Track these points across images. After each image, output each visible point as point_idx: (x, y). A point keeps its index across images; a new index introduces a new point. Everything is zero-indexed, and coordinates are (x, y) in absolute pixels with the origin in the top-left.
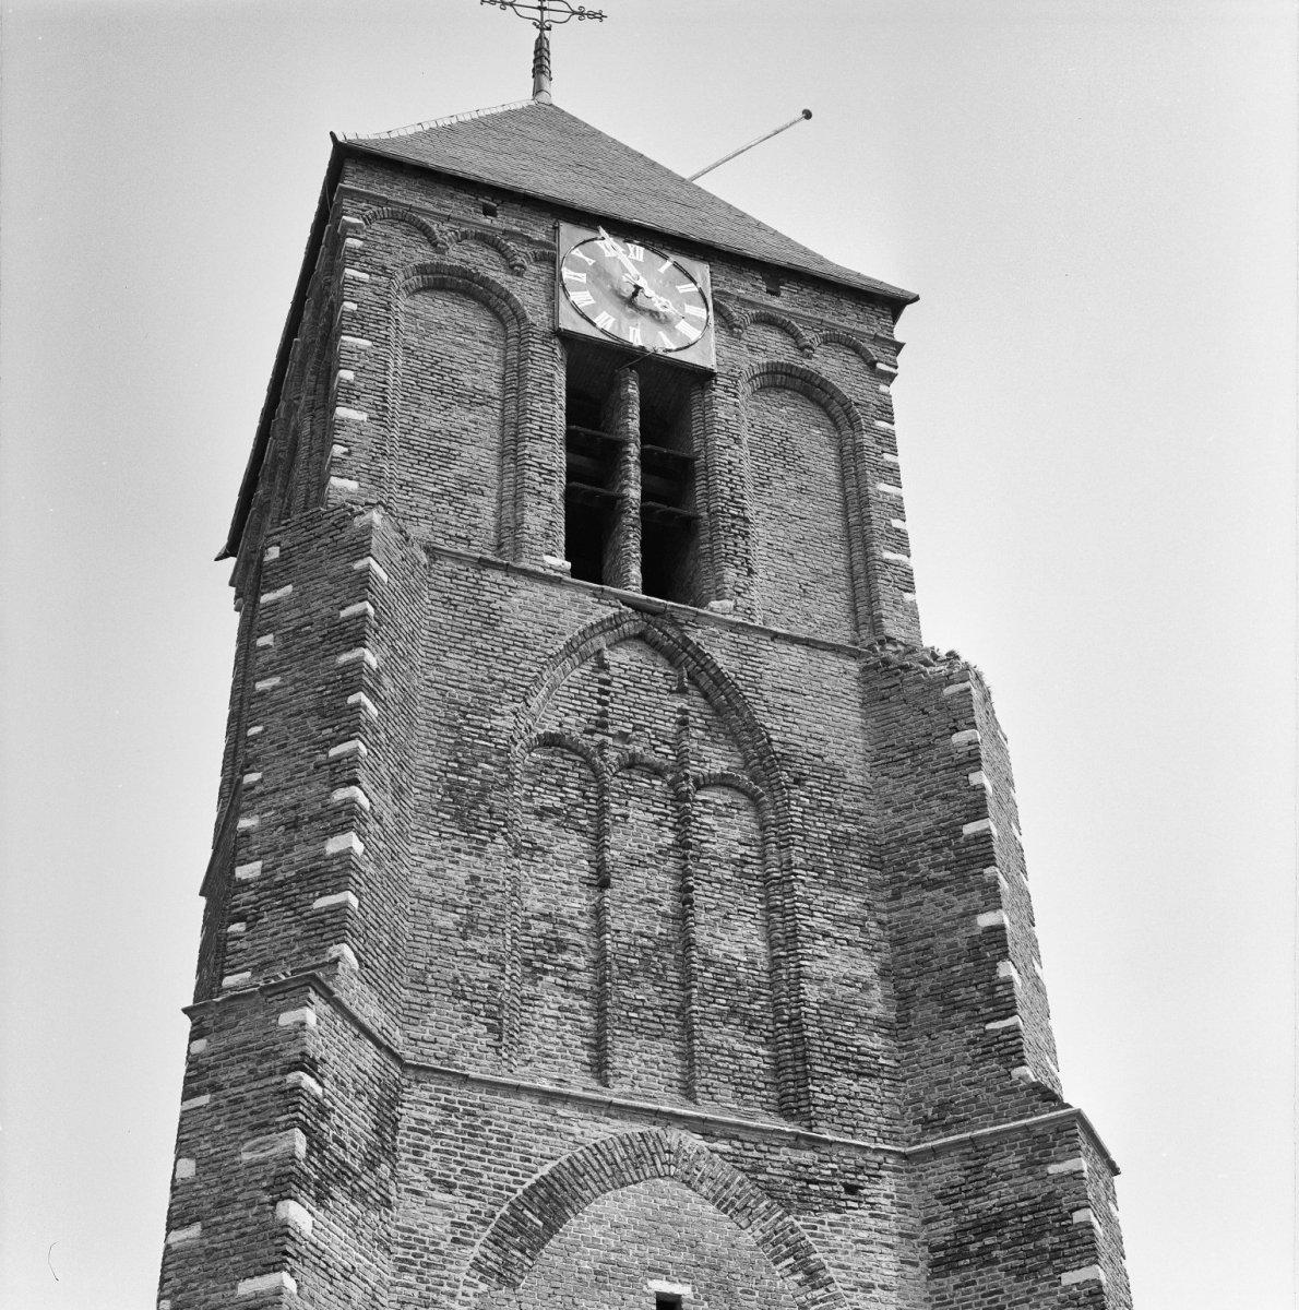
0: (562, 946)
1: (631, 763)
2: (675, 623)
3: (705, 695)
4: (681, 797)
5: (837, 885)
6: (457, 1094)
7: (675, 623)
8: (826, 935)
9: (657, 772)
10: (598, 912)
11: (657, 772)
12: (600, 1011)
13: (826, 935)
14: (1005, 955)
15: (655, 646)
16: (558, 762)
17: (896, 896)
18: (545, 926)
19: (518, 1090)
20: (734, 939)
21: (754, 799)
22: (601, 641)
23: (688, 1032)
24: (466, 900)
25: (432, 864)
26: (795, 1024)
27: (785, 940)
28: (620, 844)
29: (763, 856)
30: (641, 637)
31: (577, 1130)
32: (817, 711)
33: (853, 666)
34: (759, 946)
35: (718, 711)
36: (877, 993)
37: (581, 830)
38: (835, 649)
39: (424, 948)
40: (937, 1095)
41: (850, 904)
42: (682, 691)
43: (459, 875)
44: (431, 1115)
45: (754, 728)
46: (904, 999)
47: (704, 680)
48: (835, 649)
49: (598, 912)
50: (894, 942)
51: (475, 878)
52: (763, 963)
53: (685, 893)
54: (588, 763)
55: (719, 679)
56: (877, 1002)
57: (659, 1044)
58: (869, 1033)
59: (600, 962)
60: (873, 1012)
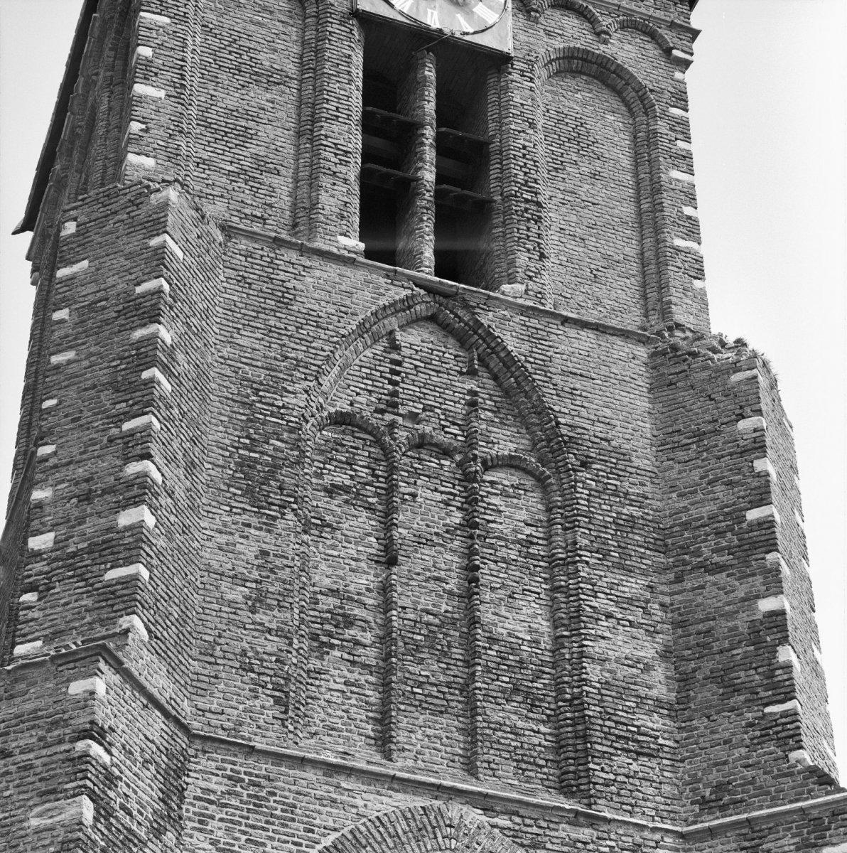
0: (349, 622)
1: (421, 443)
2: (466, 306)
3: (495, 378)
4: (469, 478)
5: (621, 567)
6: (244, 765)
7: (466, 306)
8: (609, 616)
9: (446, 452)
10: (385, 589)
11: (446, 452)
12: (385, 686)
13: (609, 616)
14: (784, 640)
15: (446, 328)
16: (348, 440)
17: (679, 579)
18: (332, 602)
19: (302, 762)
20: (520, 619)
21: (541, 481)
22: (393, 322)
23: (471, 710)
24: (255, 574)
25: (222, 539)
26: (577, 703)
27: (569, 621)
28: (408, 522)
29: (549, 537)
30: (432, 319)
31: (360, 802)
32: (611, 400)
33: (642, 352)
34: (544, 625)
35: (507, 393)
36: (659, 673)
37: (370, 508)
38: (624, 334)
39: (213, 621)
40: (715, 776)
41: (633, 586)
42: (472, 373)
43: (249, 550)
44: (218, 785)
45: (542, 411)
46: (684, 681)
47: (494, 363)
48: (624, 334)
49: (385, 589)
50: (676, 625)
51: (264, 553)
52: (546, 642)
53: (471, 572)
54: (378, 442)
55: (509, 361)
56: (659, 683)
57: (443, 720)
58: (650, 713)
59: (386, 637)
60: (654, 693)
